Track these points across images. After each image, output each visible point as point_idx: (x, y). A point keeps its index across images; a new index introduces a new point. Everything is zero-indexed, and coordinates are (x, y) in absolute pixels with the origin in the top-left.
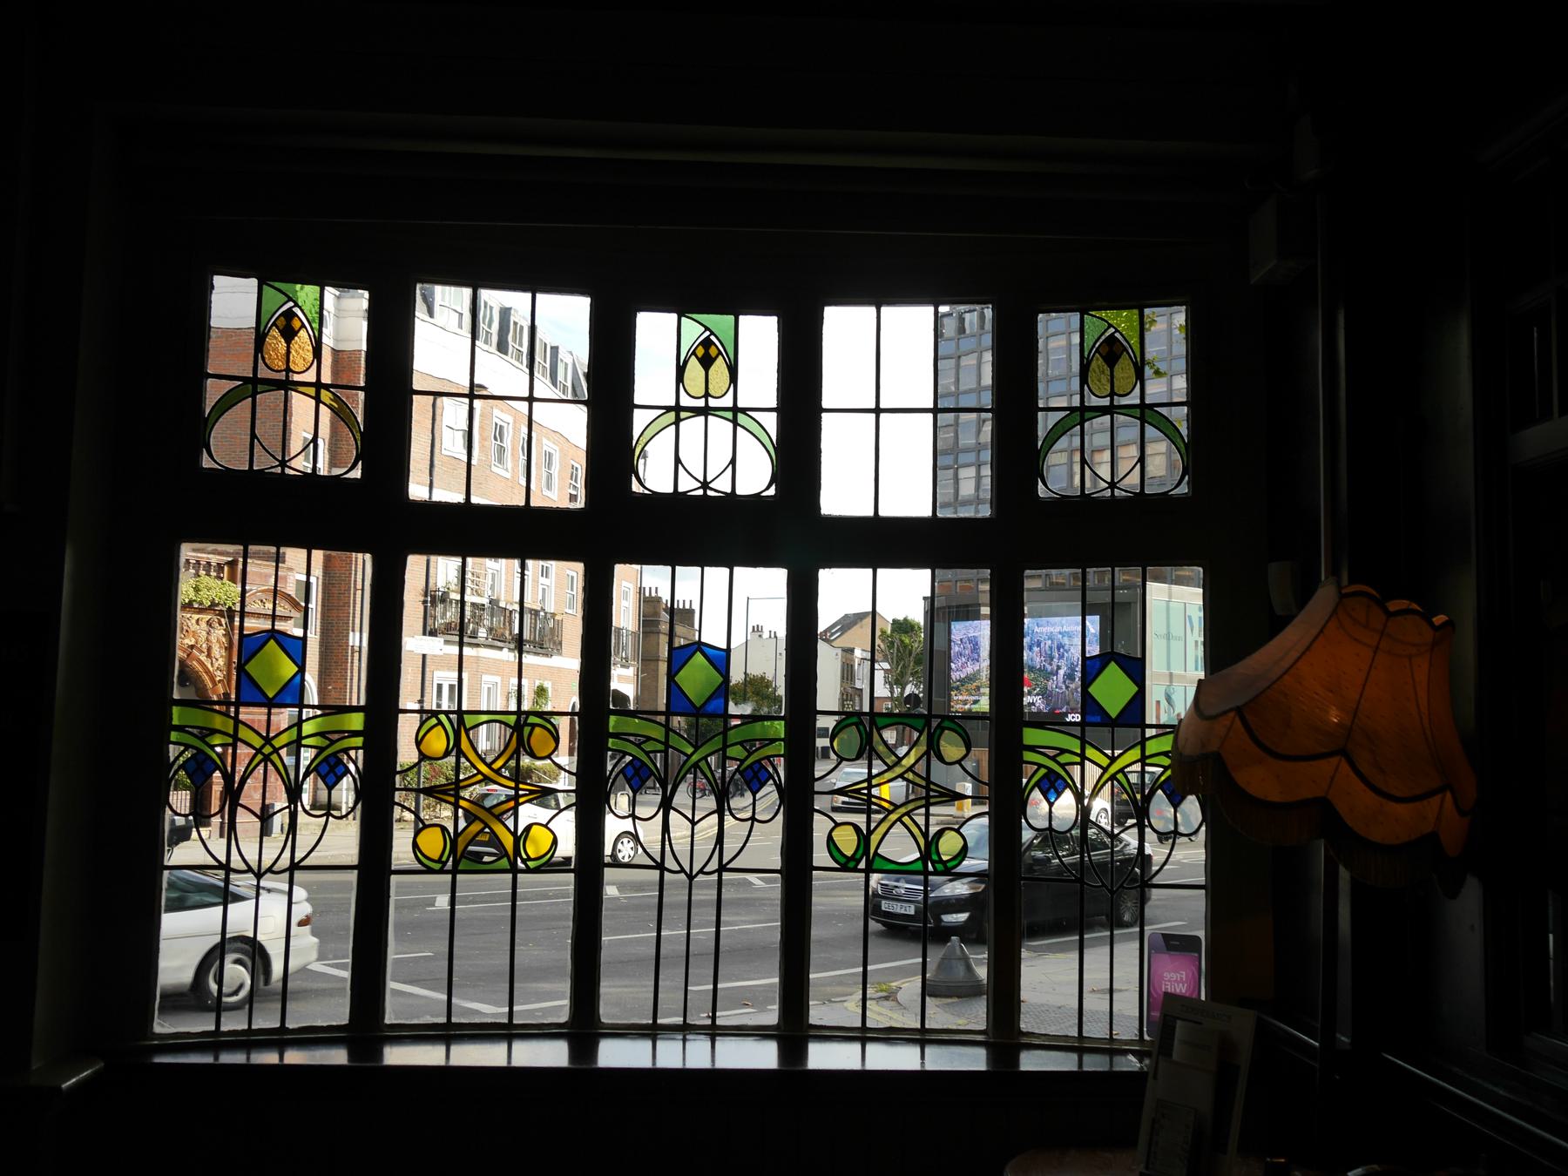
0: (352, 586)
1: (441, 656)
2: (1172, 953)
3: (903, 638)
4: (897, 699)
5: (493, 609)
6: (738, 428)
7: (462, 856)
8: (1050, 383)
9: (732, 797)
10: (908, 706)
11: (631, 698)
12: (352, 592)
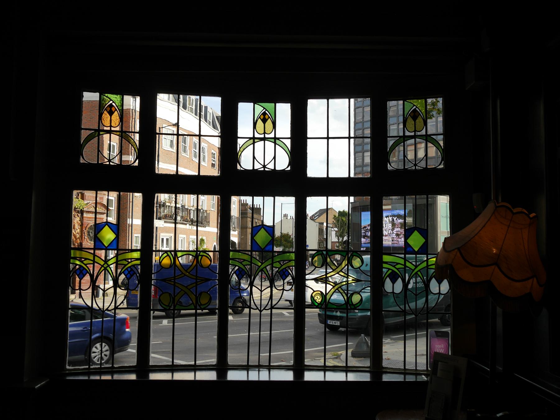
0: (128, 200)
1: (163, 227)
2: (438, 338)
3: (343, 219)
4: (341, 242)
5: (183, 209)
6: (276, 145)
7: (177, 304)
8: (399, 117)
9: (276, 281)
10: (345, 245)
11: (237, 243)
12: (128, 203)
